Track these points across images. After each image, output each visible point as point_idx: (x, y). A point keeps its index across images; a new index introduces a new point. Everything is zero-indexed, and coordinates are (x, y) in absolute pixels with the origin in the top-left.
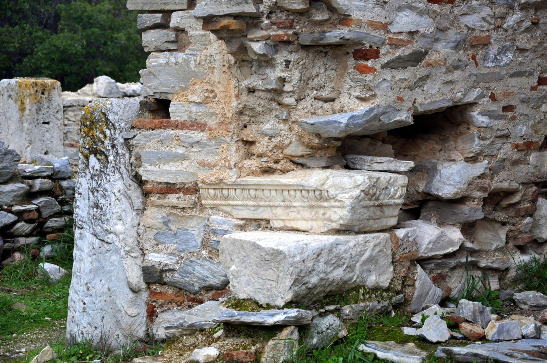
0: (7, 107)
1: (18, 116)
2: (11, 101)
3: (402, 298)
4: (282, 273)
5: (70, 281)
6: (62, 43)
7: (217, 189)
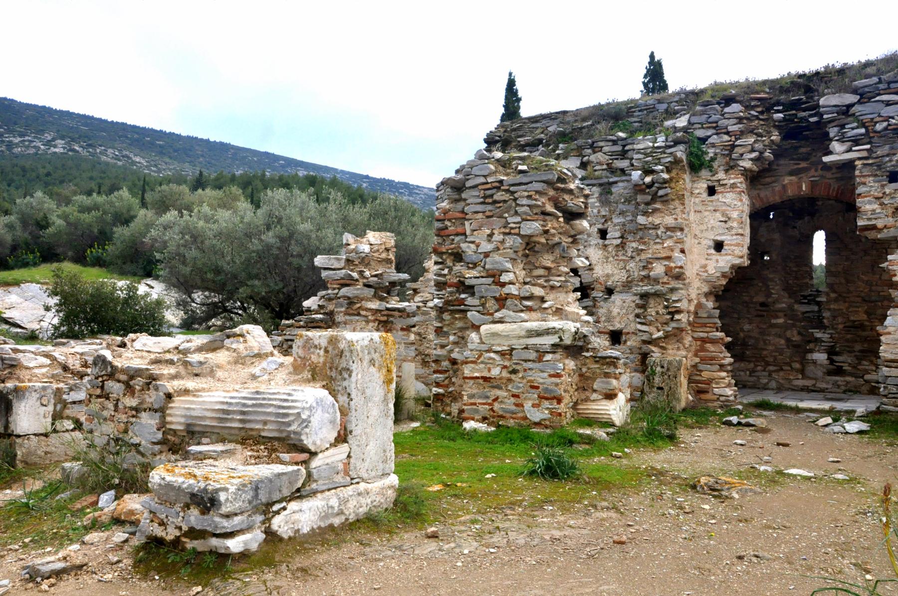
0: (367, 379)
1: (383, 394)
2: (373, 370)
3: (243, 522)
4: (783, 545)
5: (25, 265)
6: (881, 520)
7: (593, 185)
